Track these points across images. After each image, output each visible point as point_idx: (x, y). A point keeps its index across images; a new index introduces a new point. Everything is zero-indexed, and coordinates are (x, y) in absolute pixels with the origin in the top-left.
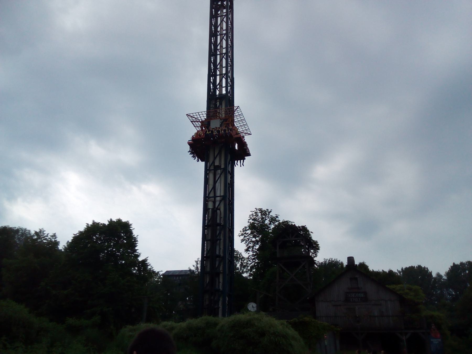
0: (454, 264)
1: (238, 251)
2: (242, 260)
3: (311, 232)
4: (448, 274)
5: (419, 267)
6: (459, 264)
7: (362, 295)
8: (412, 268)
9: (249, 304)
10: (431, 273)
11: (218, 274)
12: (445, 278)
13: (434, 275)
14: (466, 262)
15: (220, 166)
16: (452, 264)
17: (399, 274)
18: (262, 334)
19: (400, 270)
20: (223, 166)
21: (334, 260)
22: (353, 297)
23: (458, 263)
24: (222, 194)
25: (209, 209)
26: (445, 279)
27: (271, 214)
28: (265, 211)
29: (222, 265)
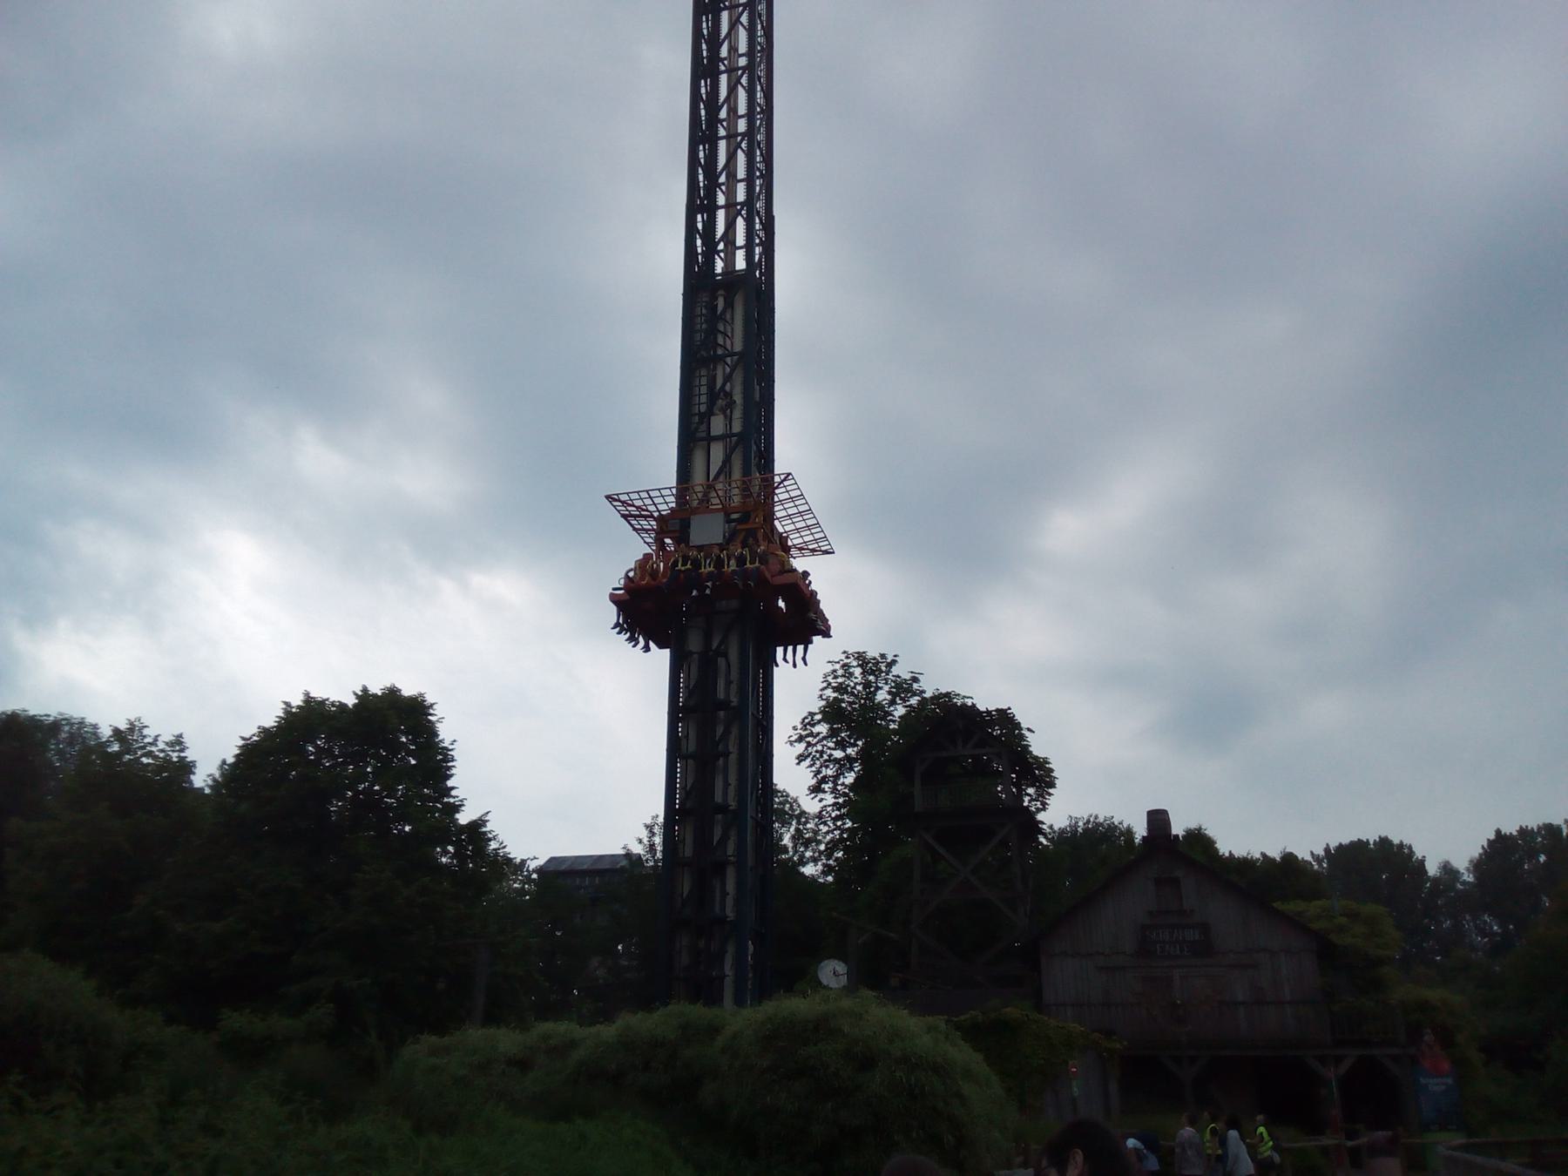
0: (1498, 832)
1: (787, 790)
3: (1029, 730)
4: (1478, 866)
5: (1384, 842)
6: (1515, 833)
8: (1358, 847)
9: (822, 964)
10: (1422, 862)
11: (720, 868)
13: (1432, 869)
14: (1539, 828)
16: (1494, 833)
21: (1105, 820)
23: (1510, 828)
25: (691, 653)
27: (895, 670)
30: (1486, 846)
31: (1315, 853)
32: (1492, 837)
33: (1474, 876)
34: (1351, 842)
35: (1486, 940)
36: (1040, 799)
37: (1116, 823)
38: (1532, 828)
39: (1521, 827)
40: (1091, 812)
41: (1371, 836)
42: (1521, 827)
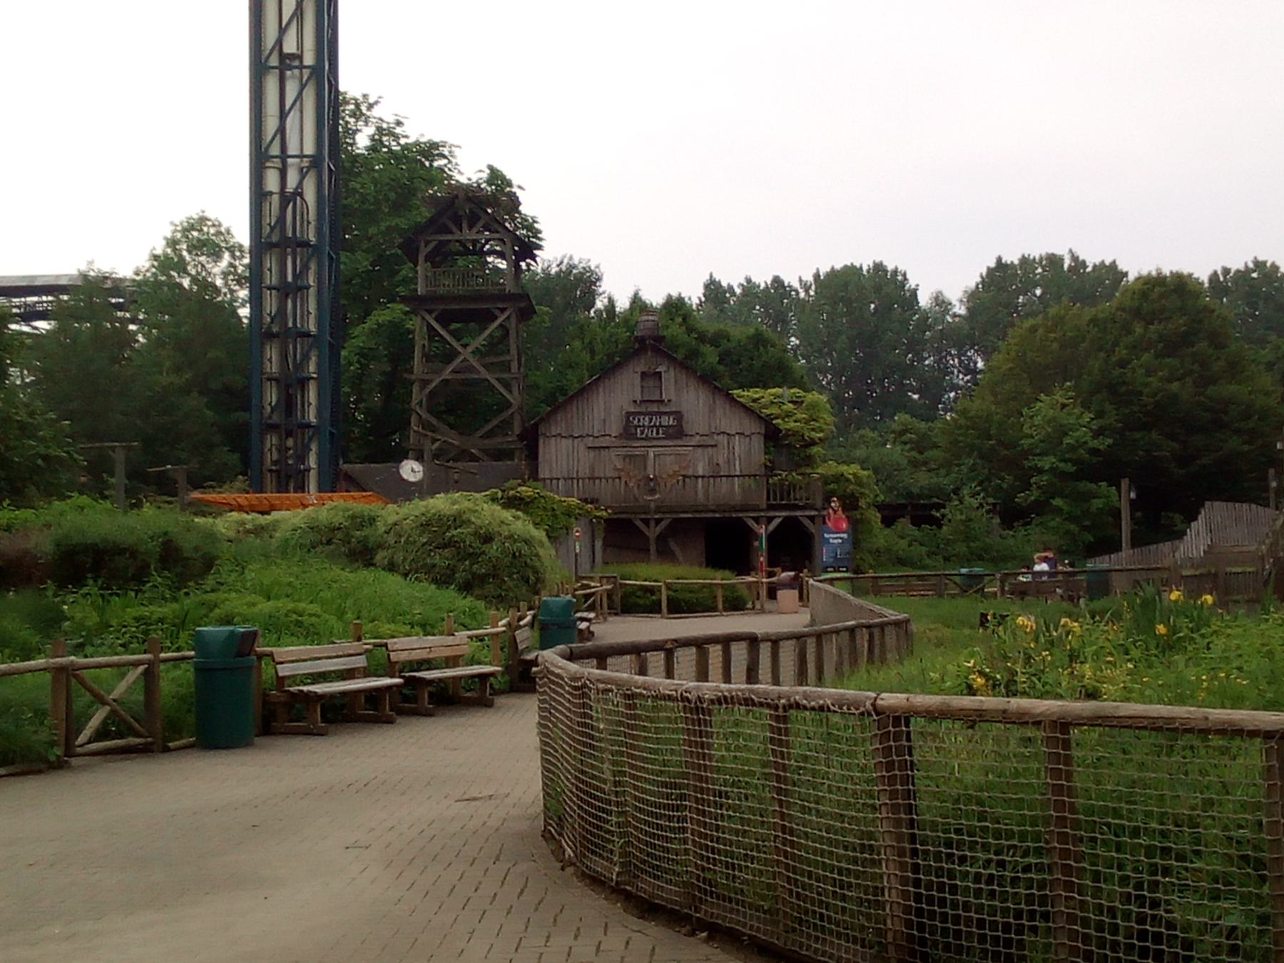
0: (999, 259)
1: (220, 220)
2: (233, 256)
3: (520, 187)
4: (973, 297)
5: (879, 268)
6: (1016, 262)
7: (668, 421)
8: (851, 272)
9: (403, 463)
10: (914, 293)
11: (303, 383)
12: (961, 310)
13: (924, 300)
14: (1041, 258)
15: (300, 57)
16: (995, 261)
17: (802, 295)
18: (488, 539)
19: (809, 278)
20: (309, 59)
21: (580, 262)
22: (644, 426)
23: (1012, 257)
24: (309, 149)
25: (271, 193)
26: (960, 316)
27: (376, 112)
28: (356, 100)
29: (314, 358)
30: (984, 274)
31: (804, 279)
32: (993, 265)
33: (968, 309)
34: (846, 266)
35: (968, 377)
36: (781, 712)
37: (593, 268)
38: (1034, 259)
39: (1023, 256)
40: (564, 253)
41: (865, 261)
42: (1023, 256)
